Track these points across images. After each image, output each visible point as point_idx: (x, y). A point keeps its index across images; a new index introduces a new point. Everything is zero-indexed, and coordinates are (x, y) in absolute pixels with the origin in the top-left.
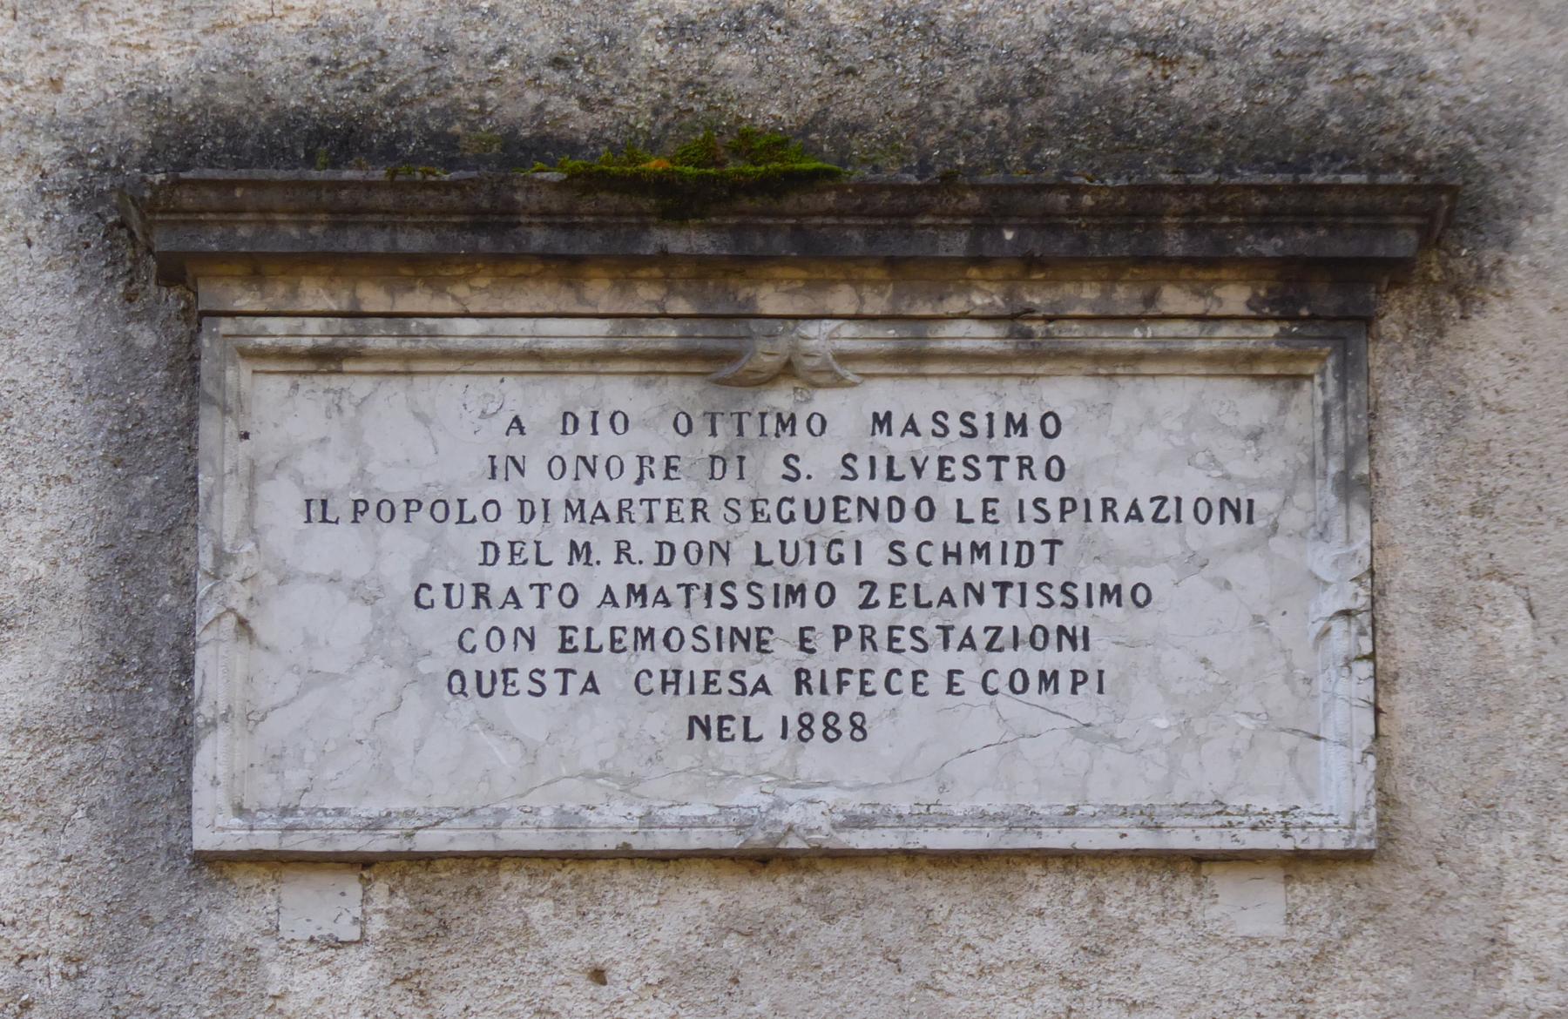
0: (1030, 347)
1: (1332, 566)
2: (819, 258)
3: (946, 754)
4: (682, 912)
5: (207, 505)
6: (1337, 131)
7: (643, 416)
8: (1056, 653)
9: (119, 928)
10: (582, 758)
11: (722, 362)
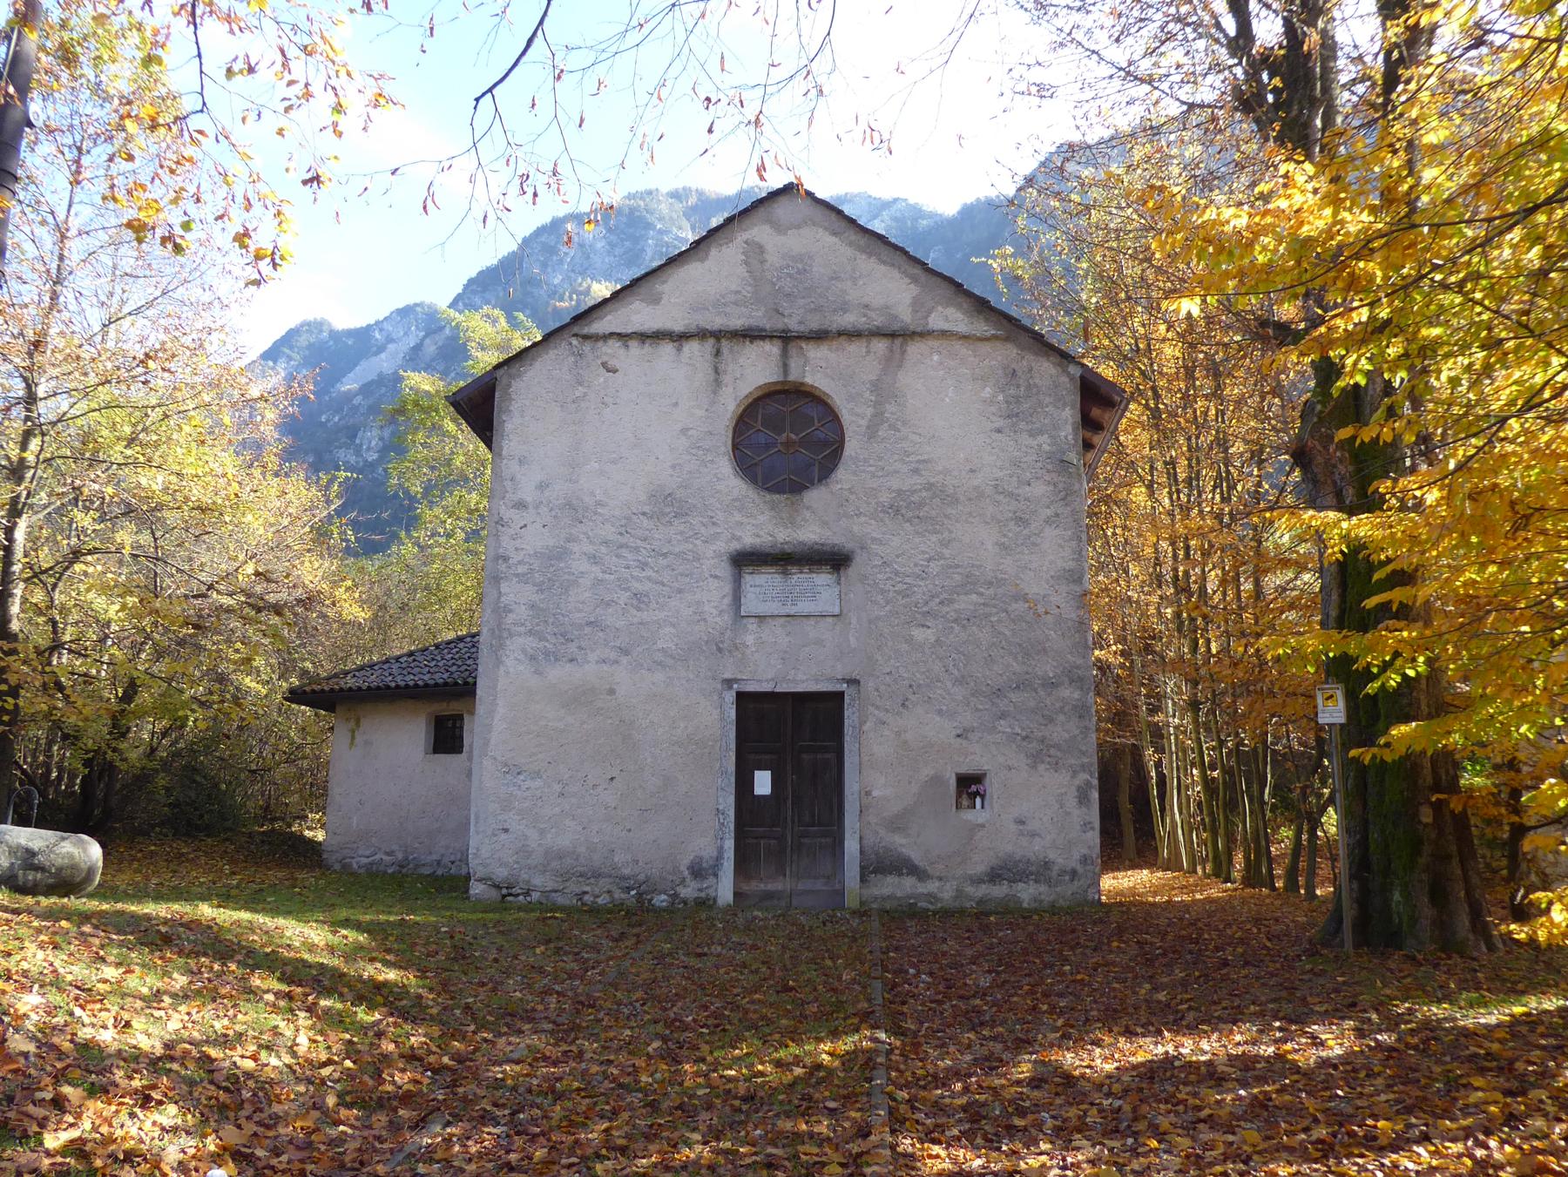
0: (811, 572)
1: (837, 590)
2: (793, 564)
3: (804, 607)
4: (782, 620)
5: (157, 940)
6: (1270, 545)
7: (778, 578)
8: (814, 598)
9: (735, 622)
10: (772, 608)
11: (785, 573)
